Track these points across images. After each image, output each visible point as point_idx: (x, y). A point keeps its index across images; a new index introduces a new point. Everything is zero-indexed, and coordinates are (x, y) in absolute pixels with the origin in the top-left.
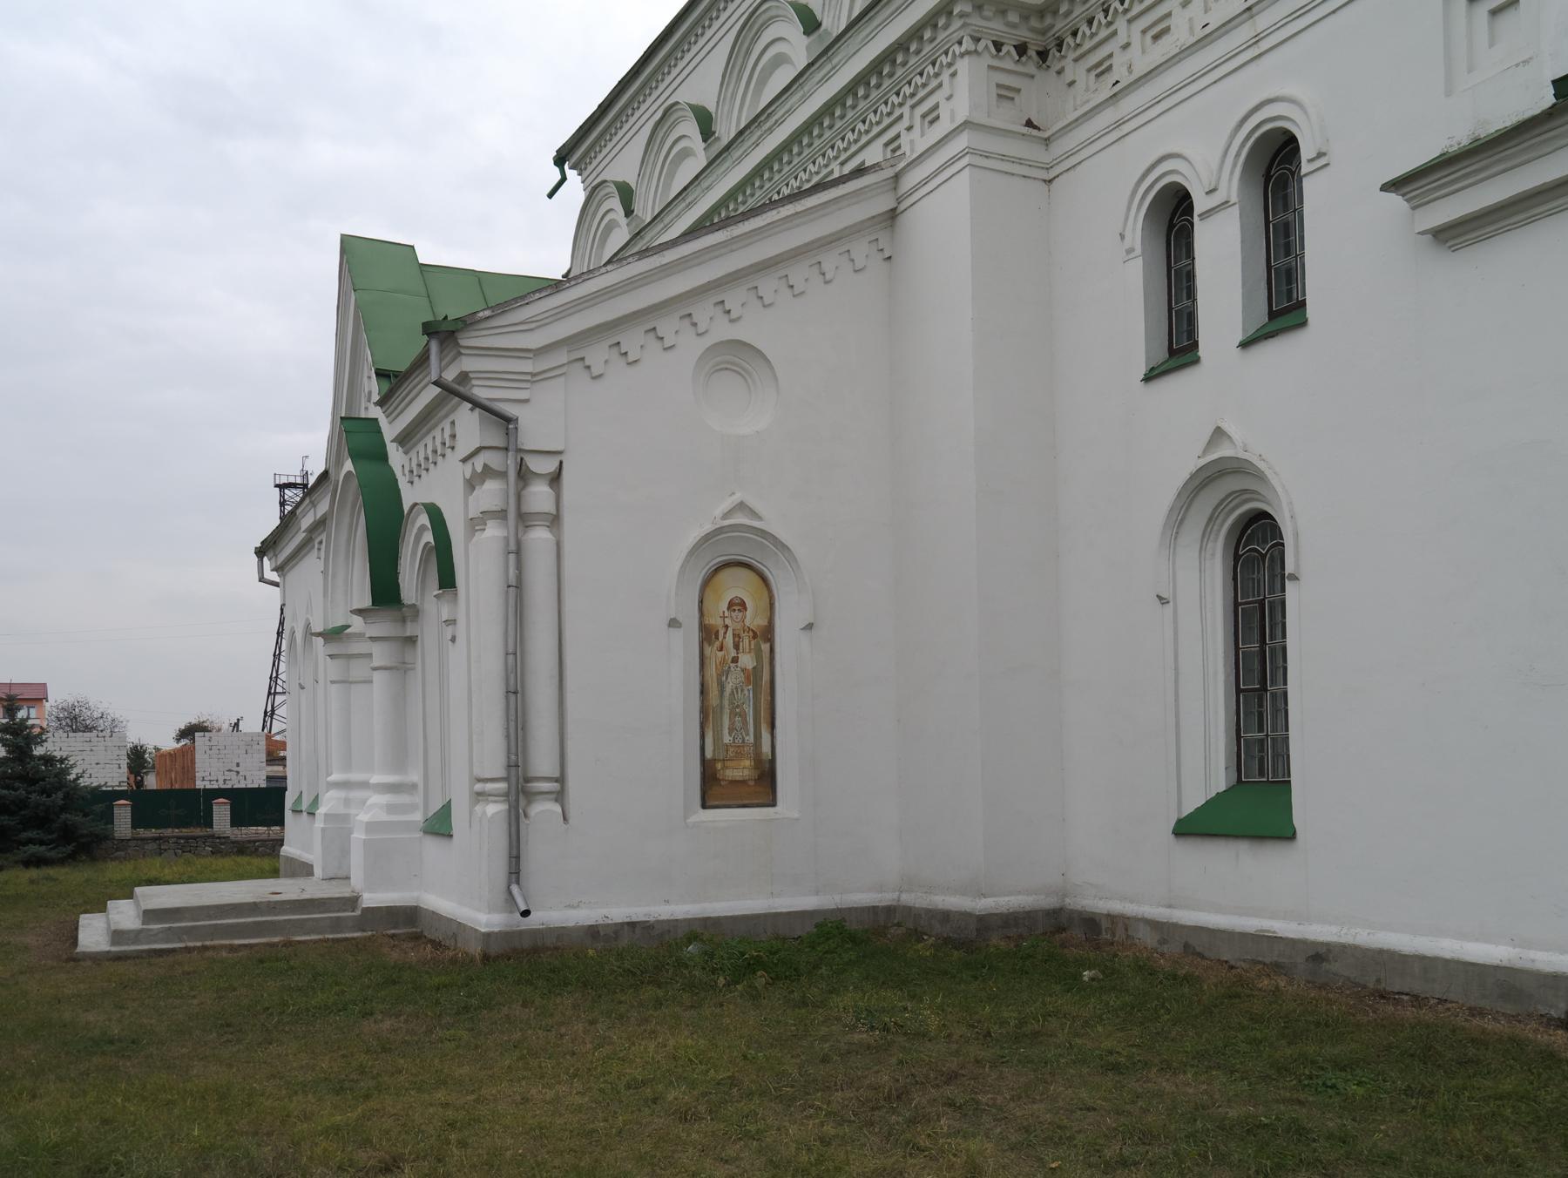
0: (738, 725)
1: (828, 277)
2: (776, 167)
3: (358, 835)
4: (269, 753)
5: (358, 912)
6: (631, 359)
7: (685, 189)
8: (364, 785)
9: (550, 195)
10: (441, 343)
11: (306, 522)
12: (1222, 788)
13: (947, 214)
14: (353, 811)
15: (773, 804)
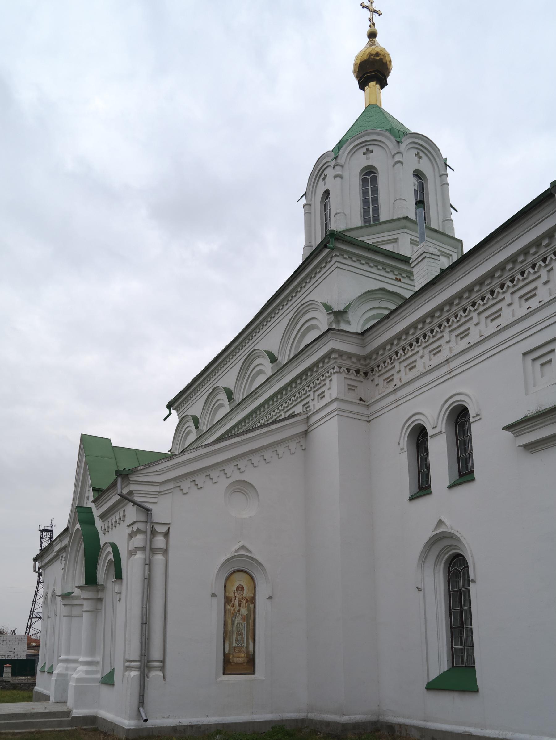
0: (239, 639)
1: (280, 456)
2: (258, 413)
3: (72, 684)
4: (28, 644)
5: (70, 718)
6: (199, 487)
7: (221, 419)
8: (76, 661)
9: (165, 420)
10: (122, 478)
11: (57, 548)
12: (446, 669)
13: (329, 433)
14: (69, 673)
15: (254, 673)
